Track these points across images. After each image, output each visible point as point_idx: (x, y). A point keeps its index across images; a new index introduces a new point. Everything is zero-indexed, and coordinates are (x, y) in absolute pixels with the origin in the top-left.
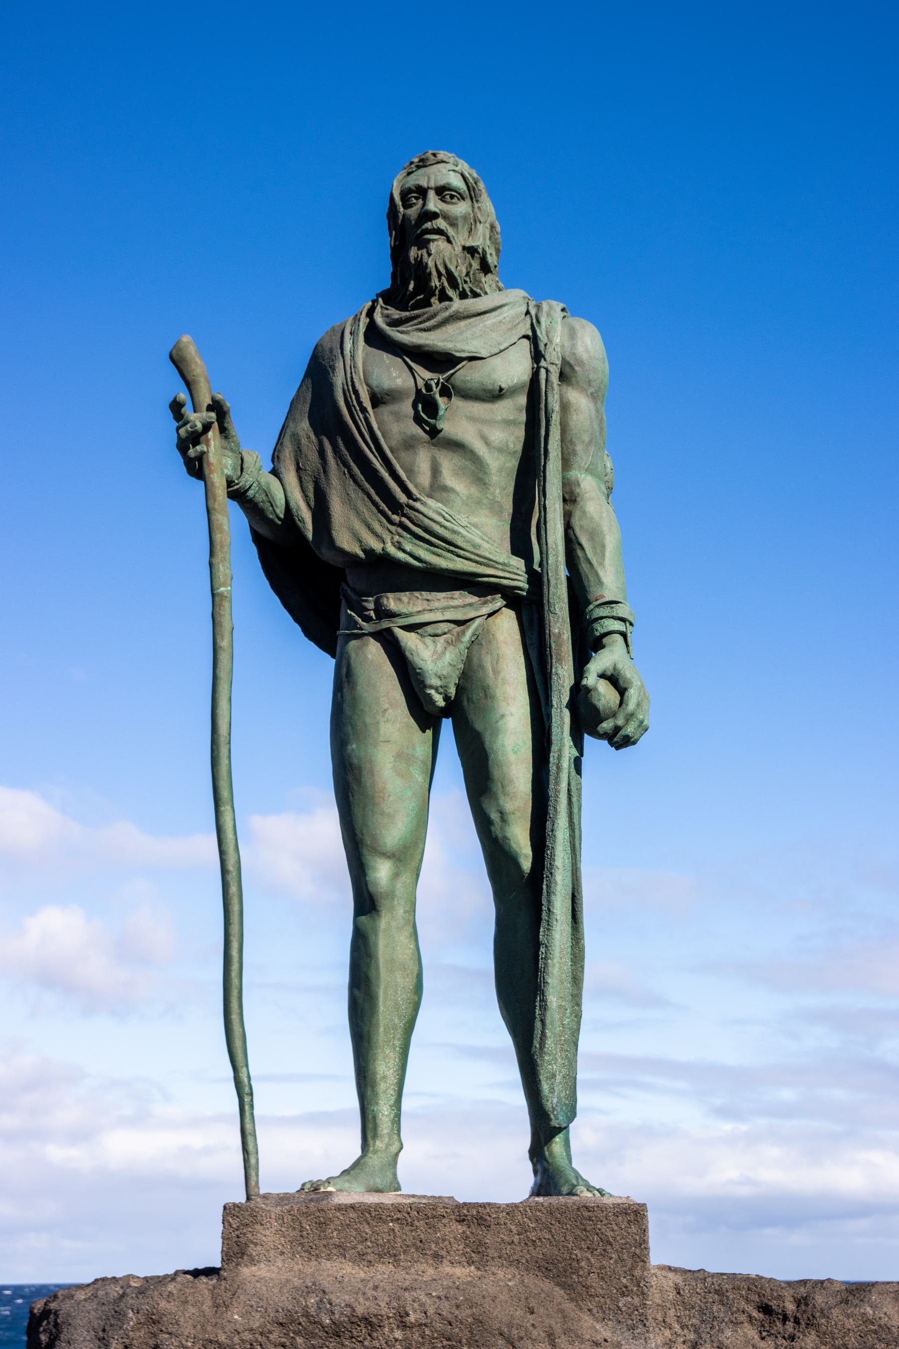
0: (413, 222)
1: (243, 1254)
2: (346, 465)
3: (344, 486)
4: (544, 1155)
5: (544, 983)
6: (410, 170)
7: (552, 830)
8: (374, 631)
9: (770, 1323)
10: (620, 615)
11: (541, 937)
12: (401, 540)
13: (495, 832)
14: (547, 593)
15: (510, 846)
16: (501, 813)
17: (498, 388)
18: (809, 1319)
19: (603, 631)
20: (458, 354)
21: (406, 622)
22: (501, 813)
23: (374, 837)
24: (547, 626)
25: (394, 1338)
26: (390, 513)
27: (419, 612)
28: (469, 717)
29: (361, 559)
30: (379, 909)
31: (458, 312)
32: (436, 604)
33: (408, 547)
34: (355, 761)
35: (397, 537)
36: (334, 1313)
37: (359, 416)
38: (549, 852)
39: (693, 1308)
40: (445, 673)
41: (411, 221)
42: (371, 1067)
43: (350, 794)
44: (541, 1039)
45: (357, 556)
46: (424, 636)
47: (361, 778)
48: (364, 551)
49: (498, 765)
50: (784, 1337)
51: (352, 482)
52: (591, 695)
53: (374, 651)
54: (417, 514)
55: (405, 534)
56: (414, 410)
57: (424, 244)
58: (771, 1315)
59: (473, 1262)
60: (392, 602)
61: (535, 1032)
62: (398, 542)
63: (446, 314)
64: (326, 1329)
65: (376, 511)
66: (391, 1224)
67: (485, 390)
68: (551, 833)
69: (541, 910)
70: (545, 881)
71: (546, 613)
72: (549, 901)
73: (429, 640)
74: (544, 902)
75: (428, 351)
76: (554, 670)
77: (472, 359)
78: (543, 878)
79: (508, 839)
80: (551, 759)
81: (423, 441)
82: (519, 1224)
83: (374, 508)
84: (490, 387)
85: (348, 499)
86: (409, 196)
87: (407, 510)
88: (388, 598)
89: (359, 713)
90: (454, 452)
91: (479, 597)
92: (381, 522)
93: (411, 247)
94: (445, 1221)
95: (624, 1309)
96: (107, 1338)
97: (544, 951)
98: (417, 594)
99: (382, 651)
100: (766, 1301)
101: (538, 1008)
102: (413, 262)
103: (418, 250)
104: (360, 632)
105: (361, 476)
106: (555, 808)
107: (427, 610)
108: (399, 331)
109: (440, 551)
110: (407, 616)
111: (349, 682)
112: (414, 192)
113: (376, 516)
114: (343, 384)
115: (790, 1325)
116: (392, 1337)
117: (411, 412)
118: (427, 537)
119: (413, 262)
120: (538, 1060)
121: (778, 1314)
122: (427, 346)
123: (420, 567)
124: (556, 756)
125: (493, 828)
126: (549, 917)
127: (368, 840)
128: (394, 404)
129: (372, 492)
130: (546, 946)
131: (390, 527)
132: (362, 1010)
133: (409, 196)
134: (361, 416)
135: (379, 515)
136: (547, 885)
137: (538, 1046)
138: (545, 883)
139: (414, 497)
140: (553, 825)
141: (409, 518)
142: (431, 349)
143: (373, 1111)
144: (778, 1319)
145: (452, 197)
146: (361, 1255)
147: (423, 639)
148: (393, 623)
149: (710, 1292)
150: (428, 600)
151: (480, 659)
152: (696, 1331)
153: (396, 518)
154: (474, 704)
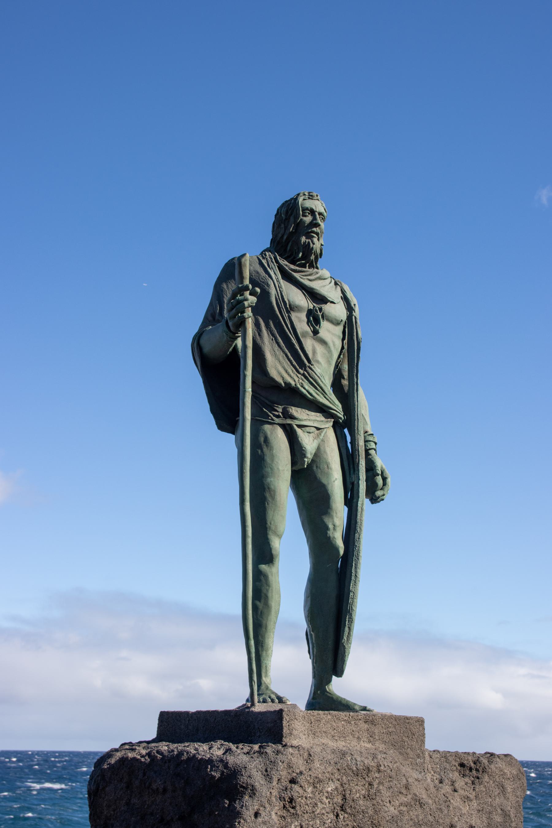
0: (306, 225)
1: (291, 734)
2: (273, 335)
4: (326, 690)
5: (352, 610)
6: (305, 198)
7: (359, 538)
8: (281, 423)
9: (464, 771)
11: (351, 588)
12: (303, 382)
13: (329, 534)
14: (357, 425)
15: (336, 542)
16: (334, 526)
17: (341, 320)
18: (483, 769)
19: (370, 447)
20: (329, 299)
21: (299, 423)
22: (334, 526)
23: (276, 527)
24: (357, 441)
25: (376, 777)
27: (305, 420)
28: (317, 475)
29: (282, 386)
30: (274, 563)
32: (312, 418)
33: (307, 387)
34: (272, 487)
35: (301, 381)
36: (357, 765)
37: (285, 314)
38: (357, 548)
39: (437, 764)
41: (305, 224)
42: (266, 641)
43: (266, 503)
44: (348, 636)
45: (281, 384)
46: (305, 432)
47: (274, 496)
48: (285, 383)
49: (335, 502)
50: (473, 777)
51: (276, 345)
52: (376, 478)
54: (312, 372)
55: (305, 380)
56: (307, 319)
58: (464, 767)
59: (371, 741)
60: (295, 411)
61: (345, 632)
62: (301, 383)
63: (318, 276)
64: (354, 772)
65: (290, 364)
66: (343, 722)
68: (358, 540)
69: (351, 575)
70: (354, 562)
71: (356, 434)
72: (356, 572)
73: (307, 434)
74: (353, 571)
75: (316, 292)
76: (360, 462)
78: (353, 560)
79: (335, 539)
80: (359, 504)
81: (310, 335)
82: (385, 725)
83: (289, 362)
85: (275, 354)
86: (306, 211)
87: (308, 369)
88: (292, 409)
89: (275, 463)
90: (322, 345)
91: (325, 418)
92: (292, 371)
93: (303, 236)
94: (361, 722)
95: (418, 764)
96: (270, 775)
97: (352, 595)
98: (304, 410)
99: (284, 434)
100: (462, 761)
101: (347, 621)
102: (302, 244)
103: (306, 238)
104: (273, 422)
105: (283, 344)
106: (360, 528)
107: (308, 420)
108: (281, 269)
109: (319, 393)
110: (300, 420)
111: (267, 445)
112: (309, 210)
113: (290, 367)
114: (275, 295)
115: (474, 772)
116: (375, 776)
117: (306, 320)
118: (316, 385)
119: (302, 244)
120: (346, 646)
121: (468, 767)
122: (317, 290)
123: (310, 398)
124: (361, 503)
125: (328, 532)
126: (356, 579)
127: (273, 527)
128: (298, 313)
129: (289, 354)
130: (354, 593)
131: (298, 374)
132: (261, 612)
133: (306, 211)
134: (287, 315)
135: (292, 366)
136: (355, 564)
137: (346, 639)
138: (354, 563)
139: (312, 363)
140: (359, 536)
141: (308, 373)
142: (318, 292)
143: (266, 663)
144: (468, 769)
146: (333, 736)
147: (304, 433)
148: (293, 422)
149: (442, 757)
150: (308, 415)
152: (439, 774)
154: (320, 469)
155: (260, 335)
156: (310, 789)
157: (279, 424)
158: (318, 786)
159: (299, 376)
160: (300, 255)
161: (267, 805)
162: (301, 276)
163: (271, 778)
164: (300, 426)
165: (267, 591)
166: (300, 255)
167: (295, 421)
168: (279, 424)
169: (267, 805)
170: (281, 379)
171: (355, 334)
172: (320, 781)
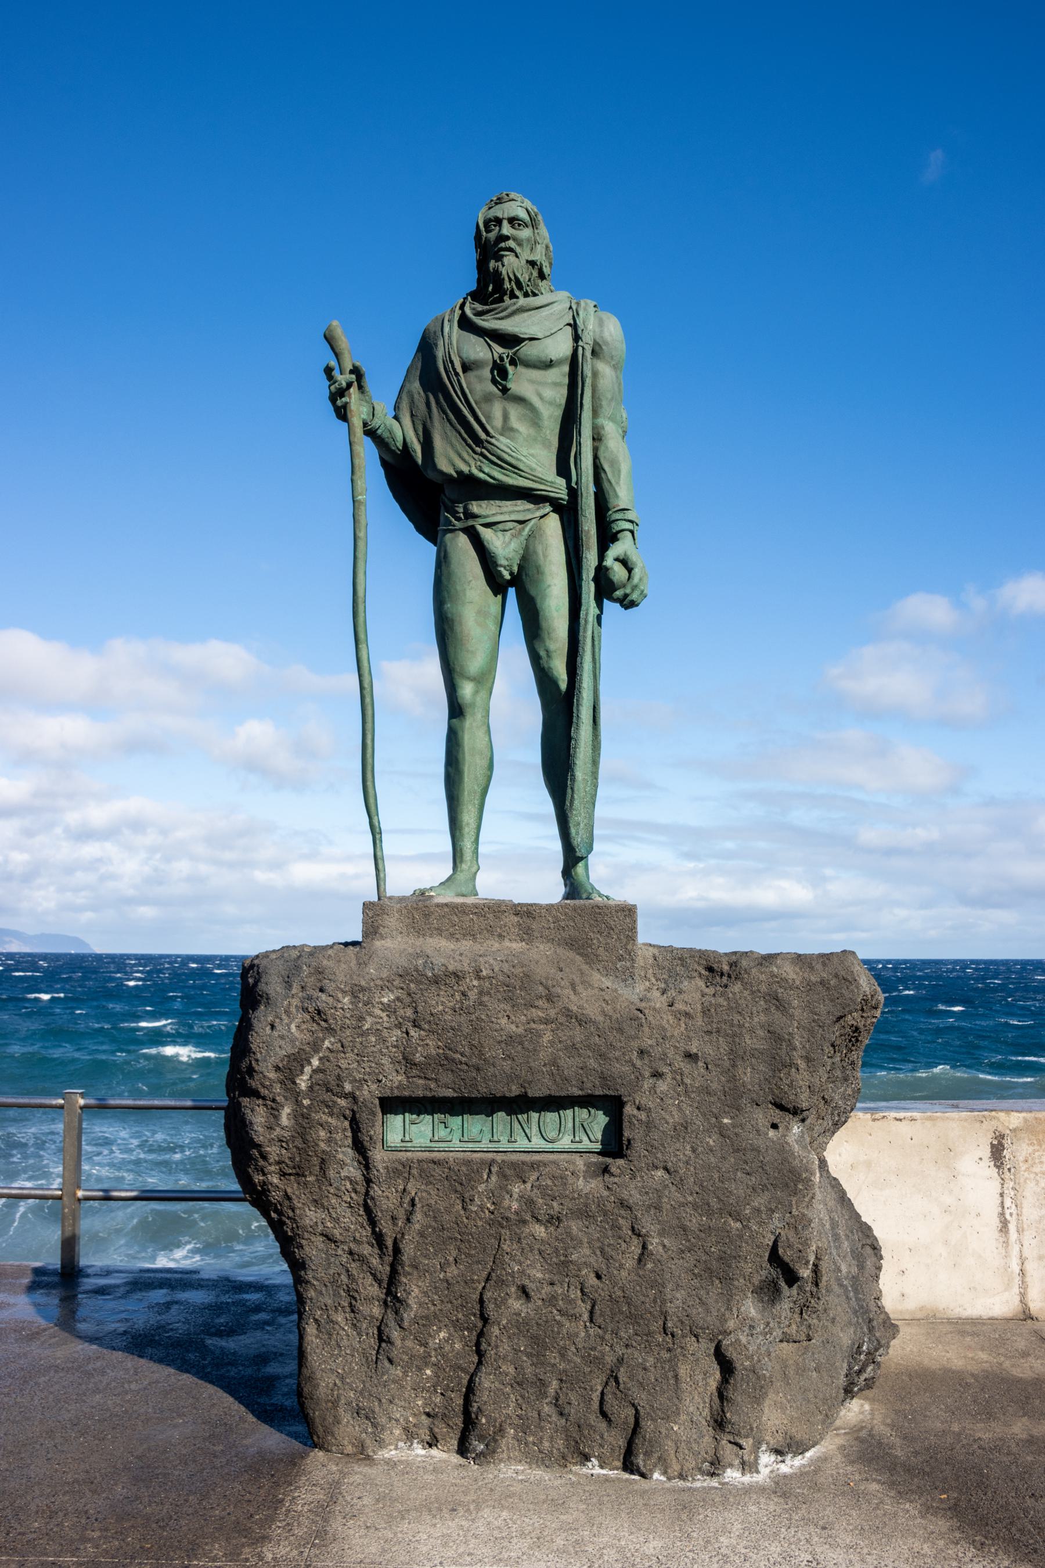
2: (444, 412)
3: (443, 427)
10: (630, 518)
12: (482, 465)
15: (553, 674)
20: (522, 336)
22: (547, 651)
26: (474, 446)
31: (522, 306)
32: (505, 509)
33: (486, 470)
34: (449, 615)
40: (510, 556)
42: (459, 817)
45: (451, 476)
48: (457, 472)
55: (484, 460)
60: (475, 507)
63: (515, 308)
67: (541, 362)
72: (578, 710)
73: (500, 534)
74: (575, 710)
77: (532, 339)
83: (463, 443)
84: (544, 359)
87: (486, 444)
98: (492, 502)
117: (490, 376)
118: (500, 463)
122: (501, 330)
127: (458, 669)
129: (462, 431)
145: (519, 225)
153: (478, 449)
155: (430, 417)
156: (346, 999)
157: (460, 529)
158: (361, 996)
159: (476, 457)
160: (490, 288)
161: (284, 1017)
162: (497, 316)
163: (291, 986)
164: (487, 525)
165: (458, 752)
166: (490, 288)
167: (477, 519)
168: (460, 529)
169: (284, 1017)
170: (452, 468)
171: (580, 373)
172: (363, 989)
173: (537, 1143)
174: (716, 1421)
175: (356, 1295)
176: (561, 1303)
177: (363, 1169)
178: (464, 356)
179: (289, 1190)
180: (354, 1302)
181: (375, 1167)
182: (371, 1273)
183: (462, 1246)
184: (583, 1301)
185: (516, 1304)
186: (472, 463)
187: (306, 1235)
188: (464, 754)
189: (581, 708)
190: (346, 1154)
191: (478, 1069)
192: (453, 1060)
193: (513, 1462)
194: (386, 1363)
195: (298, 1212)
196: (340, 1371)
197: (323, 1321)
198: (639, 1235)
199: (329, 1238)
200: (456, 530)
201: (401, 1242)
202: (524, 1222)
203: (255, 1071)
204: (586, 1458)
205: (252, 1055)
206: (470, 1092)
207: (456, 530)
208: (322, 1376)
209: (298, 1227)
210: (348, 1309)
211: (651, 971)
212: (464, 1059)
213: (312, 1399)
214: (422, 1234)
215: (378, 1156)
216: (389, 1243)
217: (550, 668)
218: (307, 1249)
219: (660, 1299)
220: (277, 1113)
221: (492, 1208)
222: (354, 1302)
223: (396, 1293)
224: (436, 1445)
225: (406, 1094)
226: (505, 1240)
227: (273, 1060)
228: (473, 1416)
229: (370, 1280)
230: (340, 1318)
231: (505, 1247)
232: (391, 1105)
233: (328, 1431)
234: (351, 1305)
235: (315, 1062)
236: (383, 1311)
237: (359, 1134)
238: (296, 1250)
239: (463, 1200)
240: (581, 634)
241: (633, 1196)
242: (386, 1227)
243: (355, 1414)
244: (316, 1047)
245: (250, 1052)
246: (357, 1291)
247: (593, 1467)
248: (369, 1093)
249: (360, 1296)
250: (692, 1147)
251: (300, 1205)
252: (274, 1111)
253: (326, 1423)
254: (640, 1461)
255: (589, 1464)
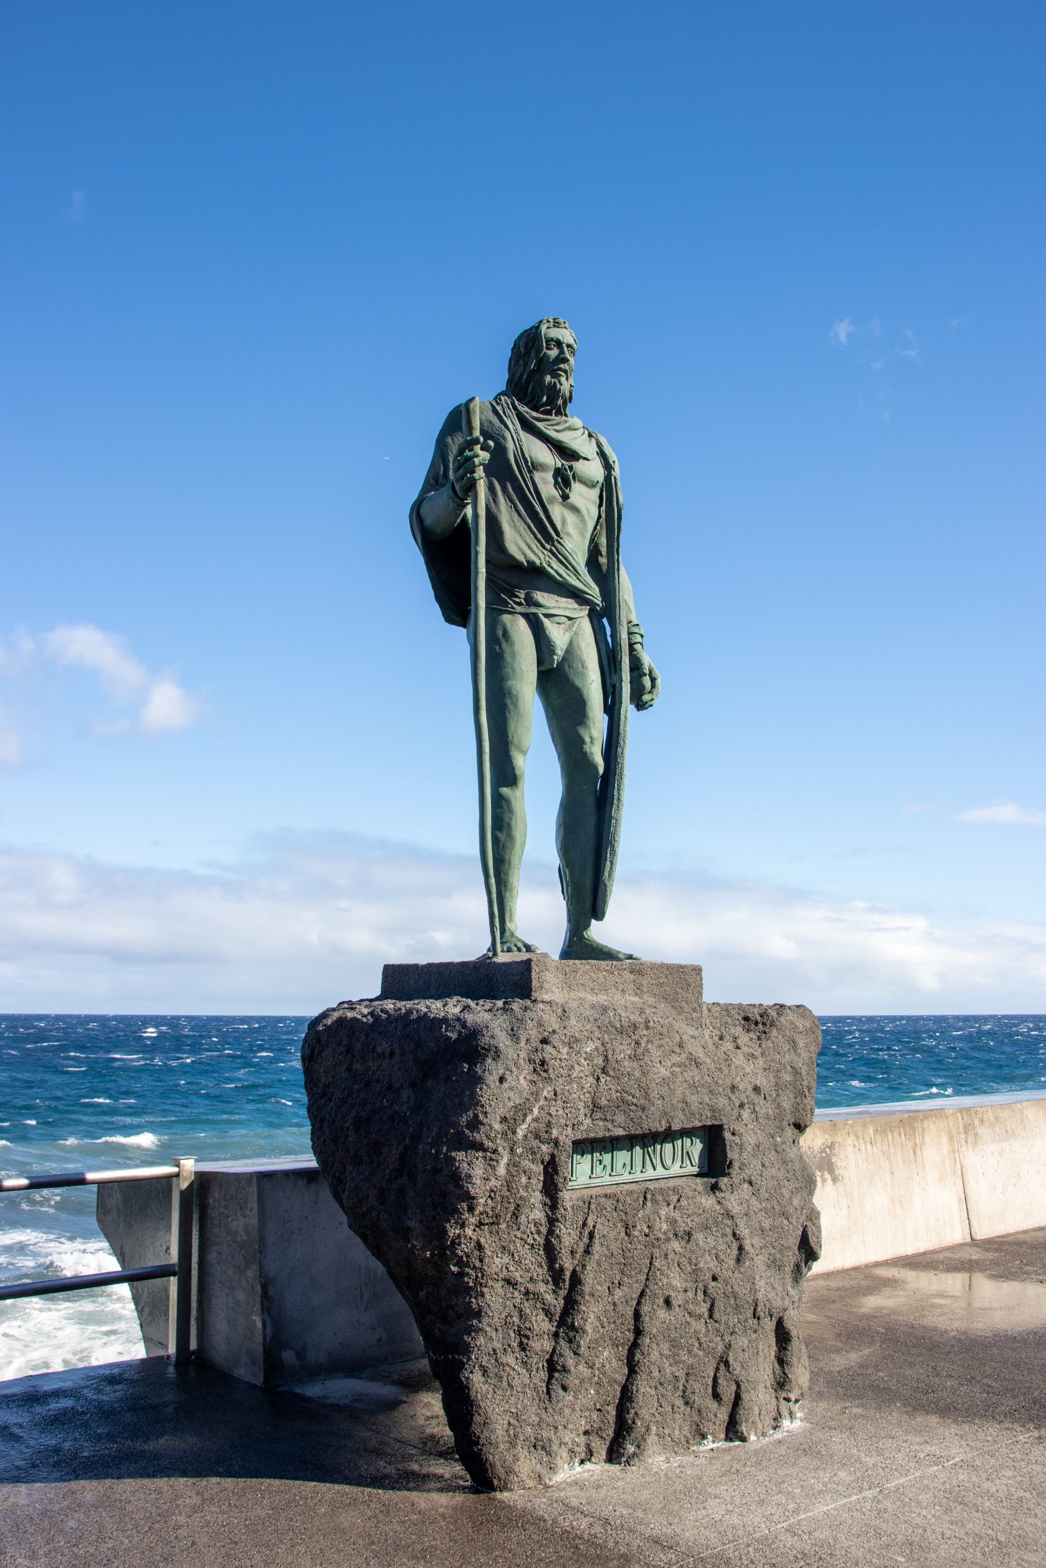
2: (512, 501)
3: (511, 516)
26: (544, 542)
32: (561, 605)
33: (555, 567)
34: (514, 692)
45: (522, 563)
48: (528, 562)
53: (522, 625)
57: (555, 375)
60: (540, 596)
63: (567, 425)
67: (590, 481)
72: (619, 794)
74: (616, 793)
82: (655, 974)
84: (593, 479)
87: (556, 543)
98: (552, 595)
110: (548, 608)
111: (506, 641)
117: (552, 481)
127: (516, 741)
129: (532, 525)
141: (556, 549)
151: (578, 642)
152: (719, 1030)
153: (548, 547)
155: (495, 501)
157: (521, 614)
158: (575, 1046)
159: (545, 552)
161: (514, 1069)
163: (518, 1039)
164: (547, 616)
169: (514, 1069)
171: (615, 499)
172: (577, 1041)
173: (660, 1172)
174: (778, 1384)
175: (528, 1333)
176: (691, 1306)
177: (547, 1210)
178: (534, 457)
179: (482, 1240)
180: (525, 1341)
181: (563, 1206)
182: (543, 1309)
183: (625, 1269)
184: (704, 1301)
185: (662, 1313)
186: (542, 556)
187: (490, 1283)
188: (516, 821)
189: (622, 792)
190: (537, 1197)
191: (643, 1109)
192: (627, 1102)
193: (656, 1455)
194: (561, 1392)
195: (487, 1260)
196: (513, 1410)
197: (490, 1366)
198: (737, 1239)
199: (508, 1282)
200: (516, 613)
201: (583, 1273)
202: (668, 1239)
203: (482, 1124)
204: (704, 1437)
205: (479, 1108)
206: (636, 1129)
207: (516, 613)
208: (497, 1419)
209: (483, 1276)
210: (517, 1349)
211: (708, 1021)
212: (635, 1101)
213: (490, 1444)
214: (599, 1264)
215: (567, 1198)
216: (568, 1275)
217: (592, 753)
218: (488, 1296)
219: (754, 1291)
220: (495, 1163)
221: (647, 1231)
222: (525, 1341)
223: (573, 1323)
224: (589, 1460)
225: (592, 1135)
226: (656, 1258)
227: (502, 1111)
228: (630, 1421)
229: (542, 1316)
230: (510, 1359)
231: (657, 1264)
232: (584, 1146)
233: (509, 1471)
234: (521, 1344)
235: (536, 1111)
236: (553, 1343)
237: (556, 1177)
238: (473, 1300)
239: (627, 1228)
240: (621, 728)
241: (736, 1209)
242: (568, 1264)
243: (532, 1448)
244: (536, 1095)
245: (477, 1104)
246: (530, 1329)
247: (709, 1444)
248: (567, 1137)
249: (532, 1333)
250: (762, 1163)
251: (490, 1254)
252: (491, 1163)
253: (508, 1463)
254: (743, 1428)
255: (705, 1442)
